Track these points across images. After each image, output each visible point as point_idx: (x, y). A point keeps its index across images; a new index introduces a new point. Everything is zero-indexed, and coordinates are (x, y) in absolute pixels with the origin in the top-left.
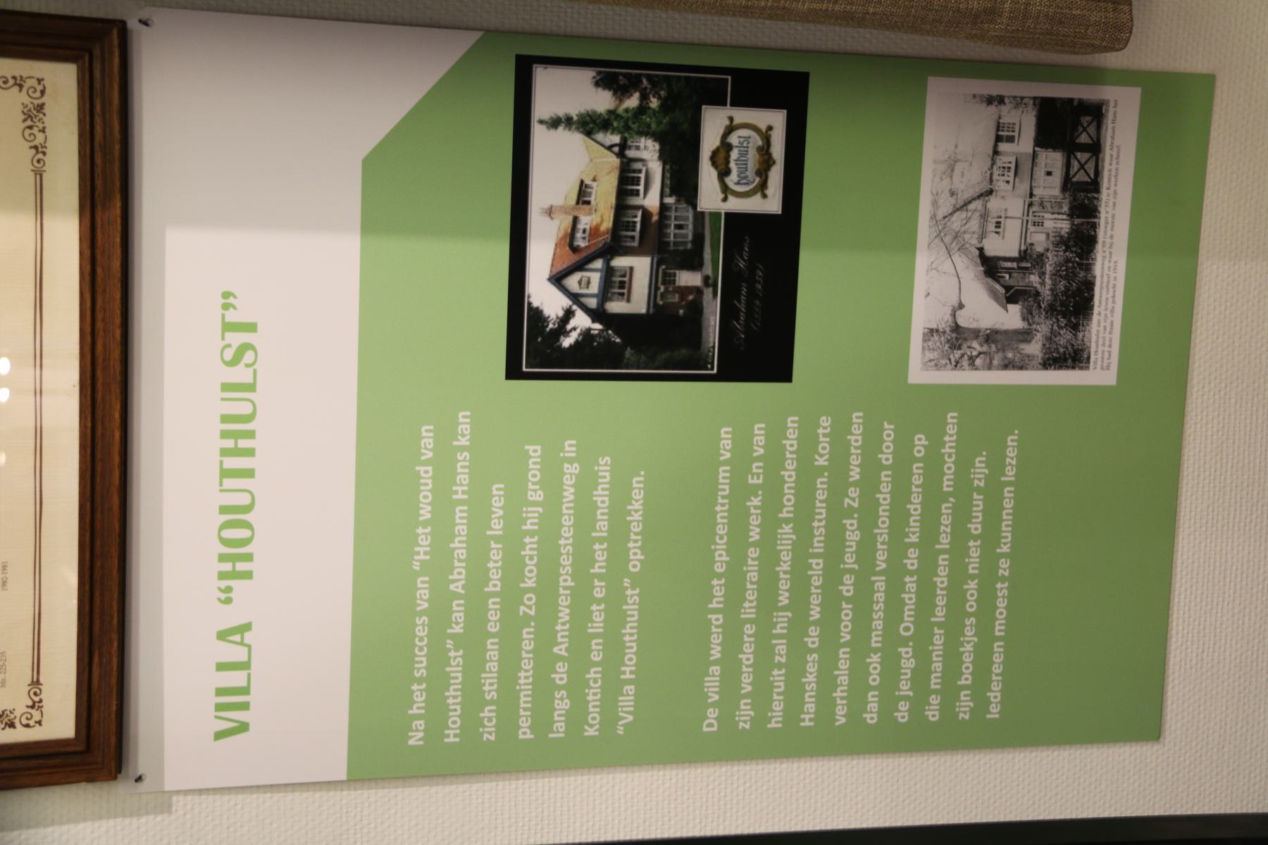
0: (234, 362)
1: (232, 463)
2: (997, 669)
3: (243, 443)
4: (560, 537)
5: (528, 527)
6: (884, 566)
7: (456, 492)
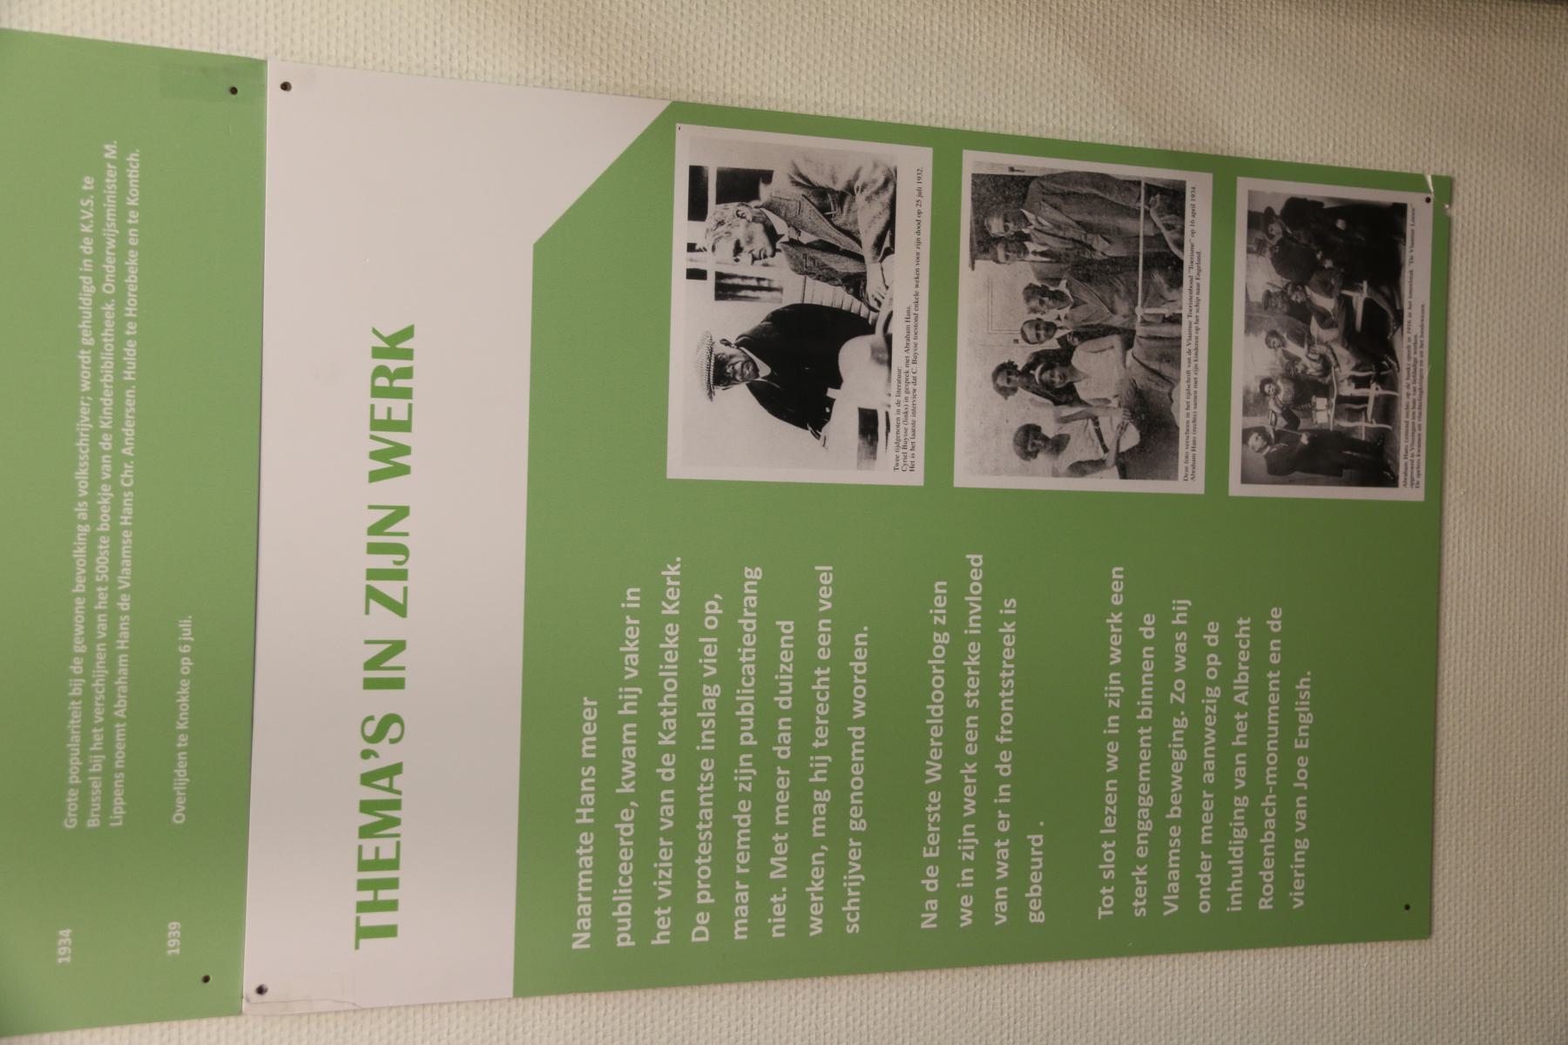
0: (391, 719)
1: (370, 919)
2: (1008, 655)
3: (384, 895)
4: (697, 855)
5: (626, 712)
6: (829, 605)
7: (580, 816)
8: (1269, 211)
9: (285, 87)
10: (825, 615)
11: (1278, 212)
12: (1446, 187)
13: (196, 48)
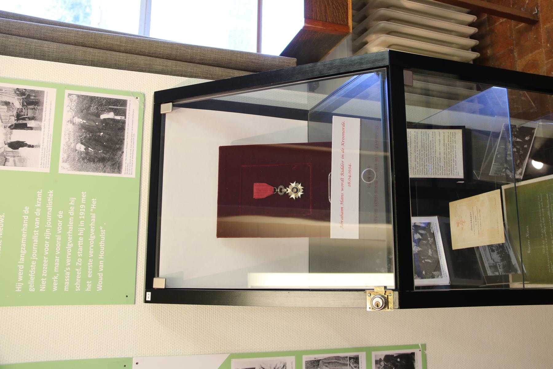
7: (17, 289)
8: (380, 359)
9: (137, 363)
10: (91, 258)
11: (383, 359)
12: (424, 346)
13: (117, 357)
